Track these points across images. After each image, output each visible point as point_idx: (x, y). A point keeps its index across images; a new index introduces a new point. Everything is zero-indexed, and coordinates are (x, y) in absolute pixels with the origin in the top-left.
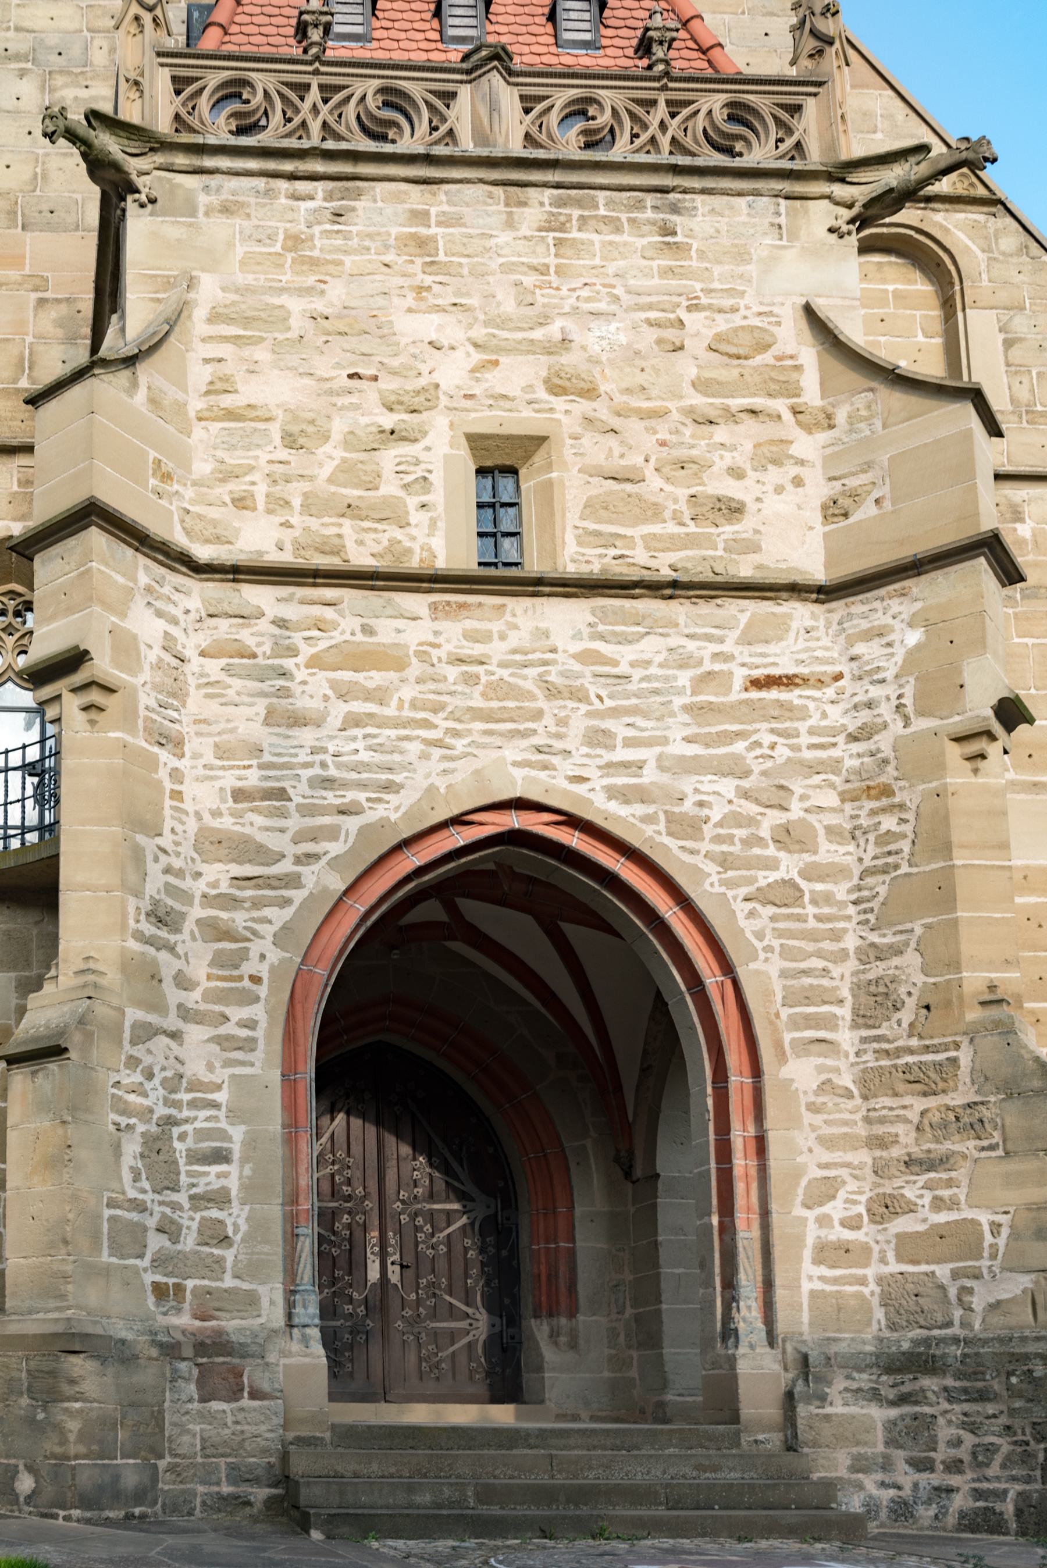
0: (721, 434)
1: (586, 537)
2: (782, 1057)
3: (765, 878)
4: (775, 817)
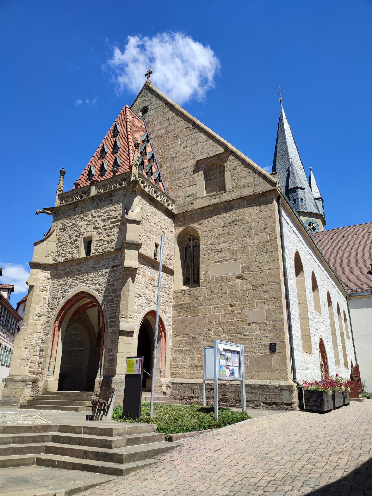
0: (113, 229)
1: (96, 250)
2: (107, 329)
3: (110, 298)
4: (113, 288)
